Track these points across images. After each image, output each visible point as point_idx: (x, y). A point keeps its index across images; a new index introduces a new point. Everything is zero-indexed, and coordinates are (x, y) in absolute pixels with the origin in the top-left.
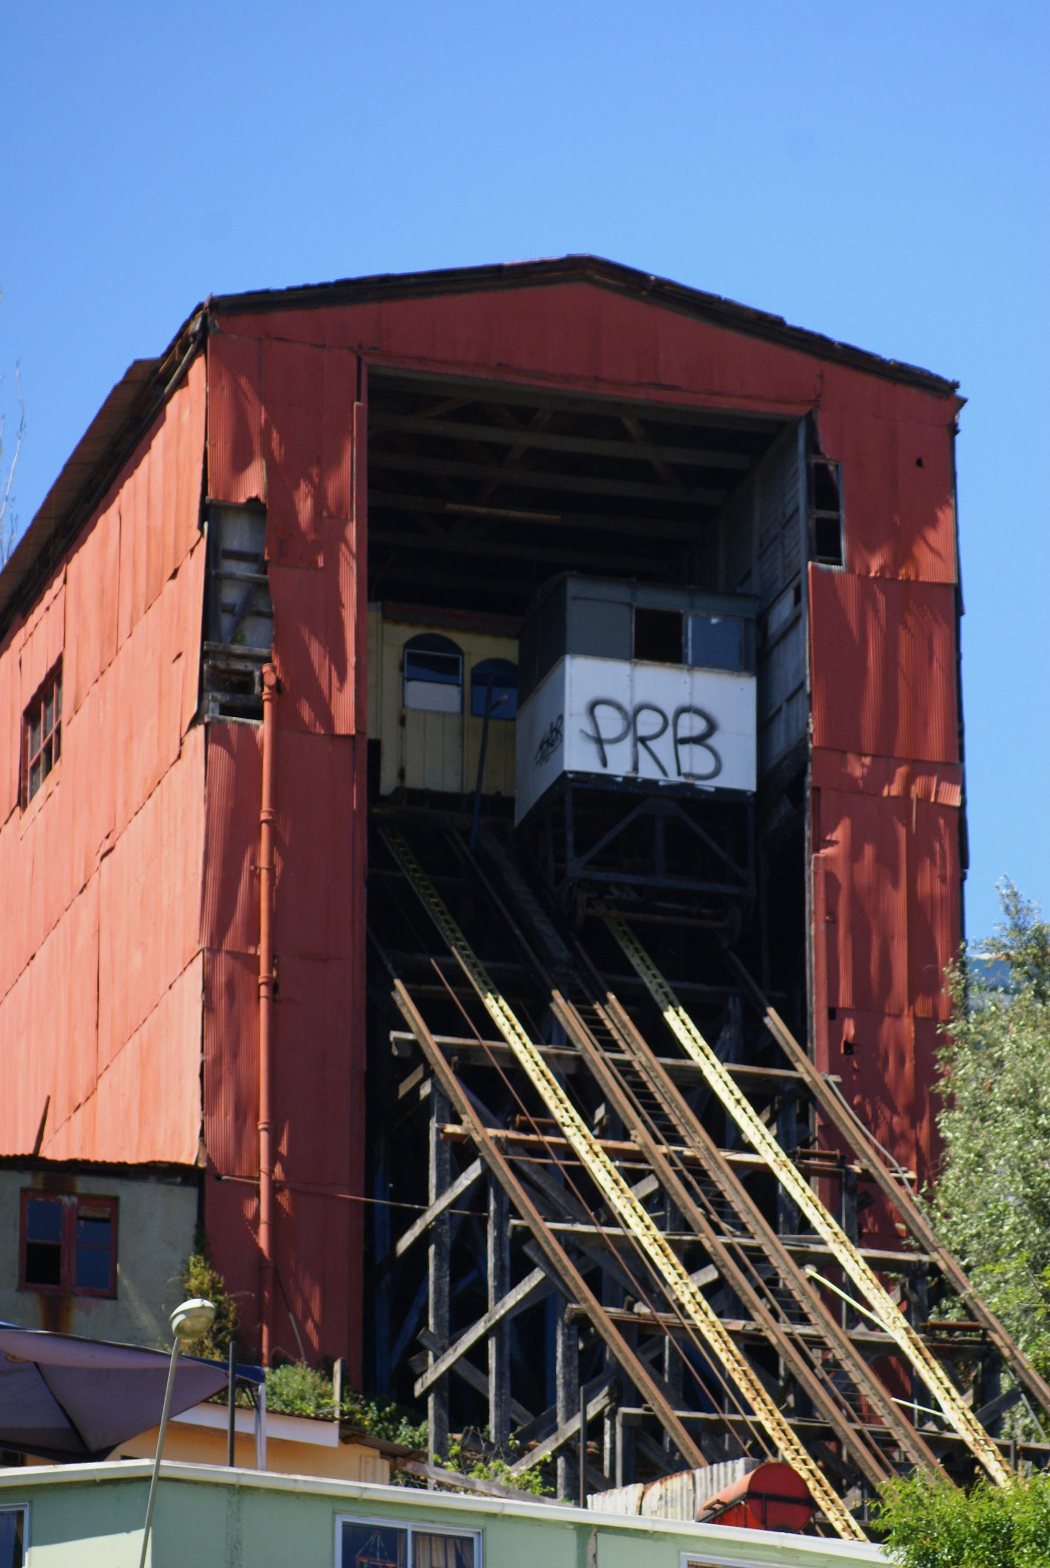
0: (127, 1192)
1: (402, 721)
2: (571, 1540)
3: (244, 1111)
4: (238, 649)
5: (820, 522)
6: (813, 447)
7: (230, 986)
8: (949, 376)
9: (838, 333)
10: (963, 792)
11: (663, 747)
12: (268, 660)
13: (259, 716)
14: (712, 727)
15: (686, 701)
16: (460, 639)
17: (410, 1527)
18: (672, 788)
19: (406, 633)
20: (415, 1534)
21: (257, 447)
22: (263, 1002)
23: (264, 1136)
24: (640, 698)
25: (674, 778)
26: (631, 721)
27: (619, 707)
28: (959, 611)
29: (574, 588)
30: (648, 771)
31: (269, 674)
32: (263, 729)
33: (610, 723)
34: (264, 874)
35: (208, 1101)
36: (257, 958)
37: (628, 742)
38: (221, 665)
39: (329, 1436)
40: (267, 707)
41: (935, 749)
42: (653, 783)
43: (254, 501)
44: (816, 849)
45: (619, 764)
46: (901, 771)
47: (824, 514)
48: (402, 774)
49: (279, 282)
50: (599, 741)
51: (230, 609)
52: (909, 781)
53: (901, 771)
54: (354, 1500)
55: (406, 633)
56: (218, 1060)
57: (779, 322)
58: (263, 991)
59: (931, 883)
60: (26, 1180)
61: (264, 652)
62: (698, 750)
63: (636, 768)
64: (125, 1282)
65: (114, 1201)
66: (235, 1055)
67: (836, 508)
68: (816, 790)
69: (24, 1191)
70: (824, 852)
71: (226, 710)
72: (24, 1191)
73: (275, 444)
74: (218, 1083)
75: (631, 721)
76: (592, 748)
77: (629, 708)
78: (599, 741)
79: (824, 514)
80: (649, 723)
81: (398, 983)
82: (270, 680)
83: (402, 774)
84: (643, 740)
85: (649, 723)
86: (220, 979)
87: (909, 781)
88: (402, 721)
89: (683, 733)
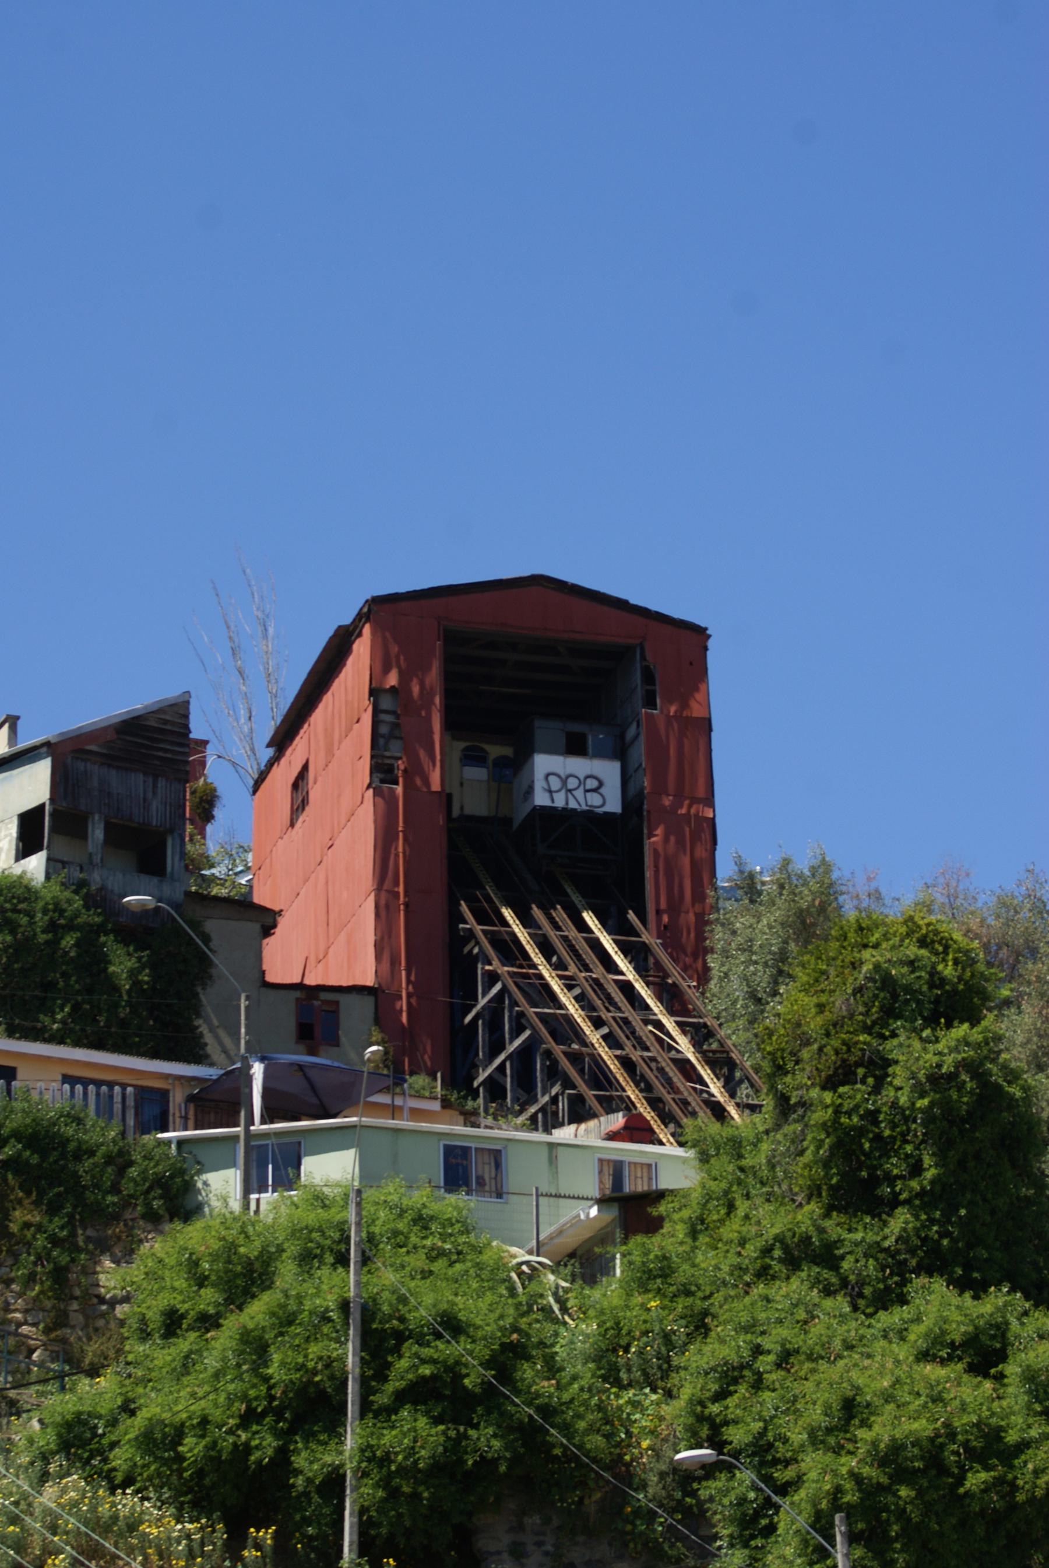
0: (343, 999)
1: (462, 784)
2: (544, 1151)
3: (394, 962)
4: (387, 754)
5: (647, 691)
6: (643, 658)
7: (387, 906)
8: (703, 625)
9: (653, 606)
10: (714, 811)
11: (579, 794)
12: (400, 758)
13: (397, 783)
14: (601, 784)
15: (589, 773)
16: (486, 747)
17: (473, 1145)
18: (584, 812)
19: (463, 745)
20: (476, 1149)
21: (394, 664)
22: (402, 913)
23: (404, 973)
24: (569, 771)
25: (584, 807)
26: (564, 782)
27: (558, 776)
28: (710, 730)
29: (537, 723)
30: (573, 805)
31: (401, 765)
32: (399, 789)
33: (555, 783)
34: (401, 855)
35: (378, 957)
36: (398, 893)
37: (563, 792)
38: (380, 761)
39: (436, 1106)
40: (401, 780)
41: (701, 792)
42: (574, 810)
43: (393, 687)
44: (649, 838)
45: (560, 801)
46: (687, 802)
47: (649, 687)
48: (462, 808)
49: (402, 589)
50: (550, 792)
51: (383, 736)
52: (690, 807)
53: (687, 802)
54: (448, 1134)
55: (463, 745)
56: (382, 939)
57: (626, 602)
58: (402, 907)
59: (701, 852)
60: (298, 994)
61: (399, 755)
62: (595, 795)
63: (567, 803)
64: (343, 1039)
65: (337, 1003)
66: (390, 937)
67: (654, 684)
68: (649, 812)
69: (297, 999)
70: (653, 839)
71: (382, 781)
72: (297, 999)
73: (402, 661)
74: (382, 949)
75: (564, 782)
76: (547, 795)
77: (563, 776)
78: (550, 792)
79: (649, 687)
80: (572, 783)
81: (462, 903)
82: (402, 767)
83: (462, 808)
84: (570, 791)
85: (572, 783)
86: (383, 902)
87: (690, 807)
88: (462, 784)
89: (588, 787)
